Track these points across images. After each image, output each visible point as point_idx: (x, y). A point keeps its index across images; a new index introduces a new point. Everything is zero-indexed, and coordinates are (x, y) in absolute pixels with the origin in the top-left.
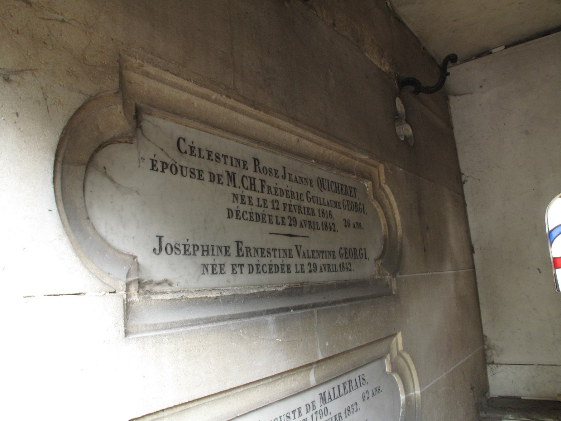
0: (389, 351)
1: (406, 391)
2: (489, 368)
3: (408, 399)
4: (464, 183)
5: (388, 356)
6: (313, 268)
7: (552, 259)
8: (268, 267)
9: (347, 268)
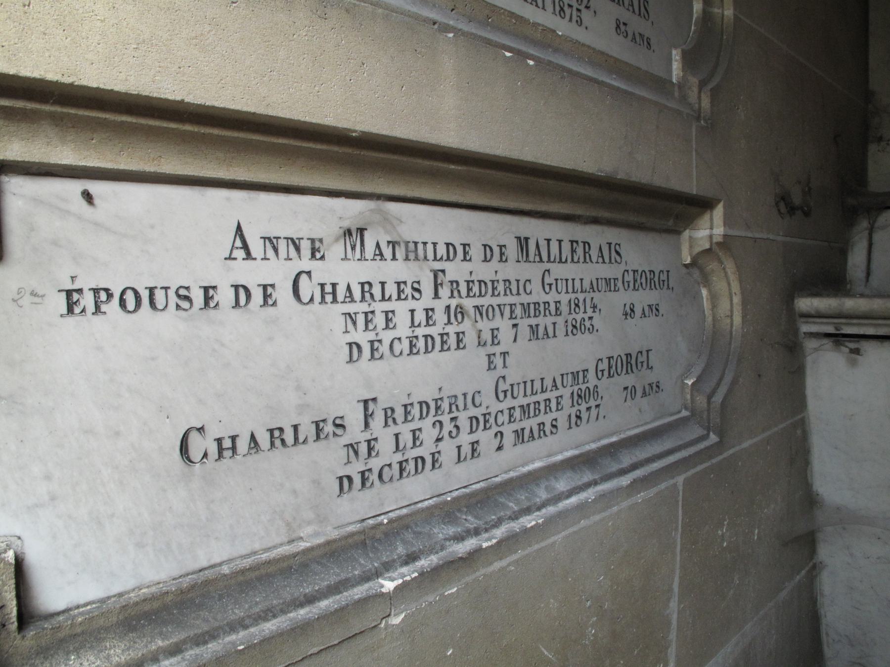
2: (873, 148)
3: (706, 16)
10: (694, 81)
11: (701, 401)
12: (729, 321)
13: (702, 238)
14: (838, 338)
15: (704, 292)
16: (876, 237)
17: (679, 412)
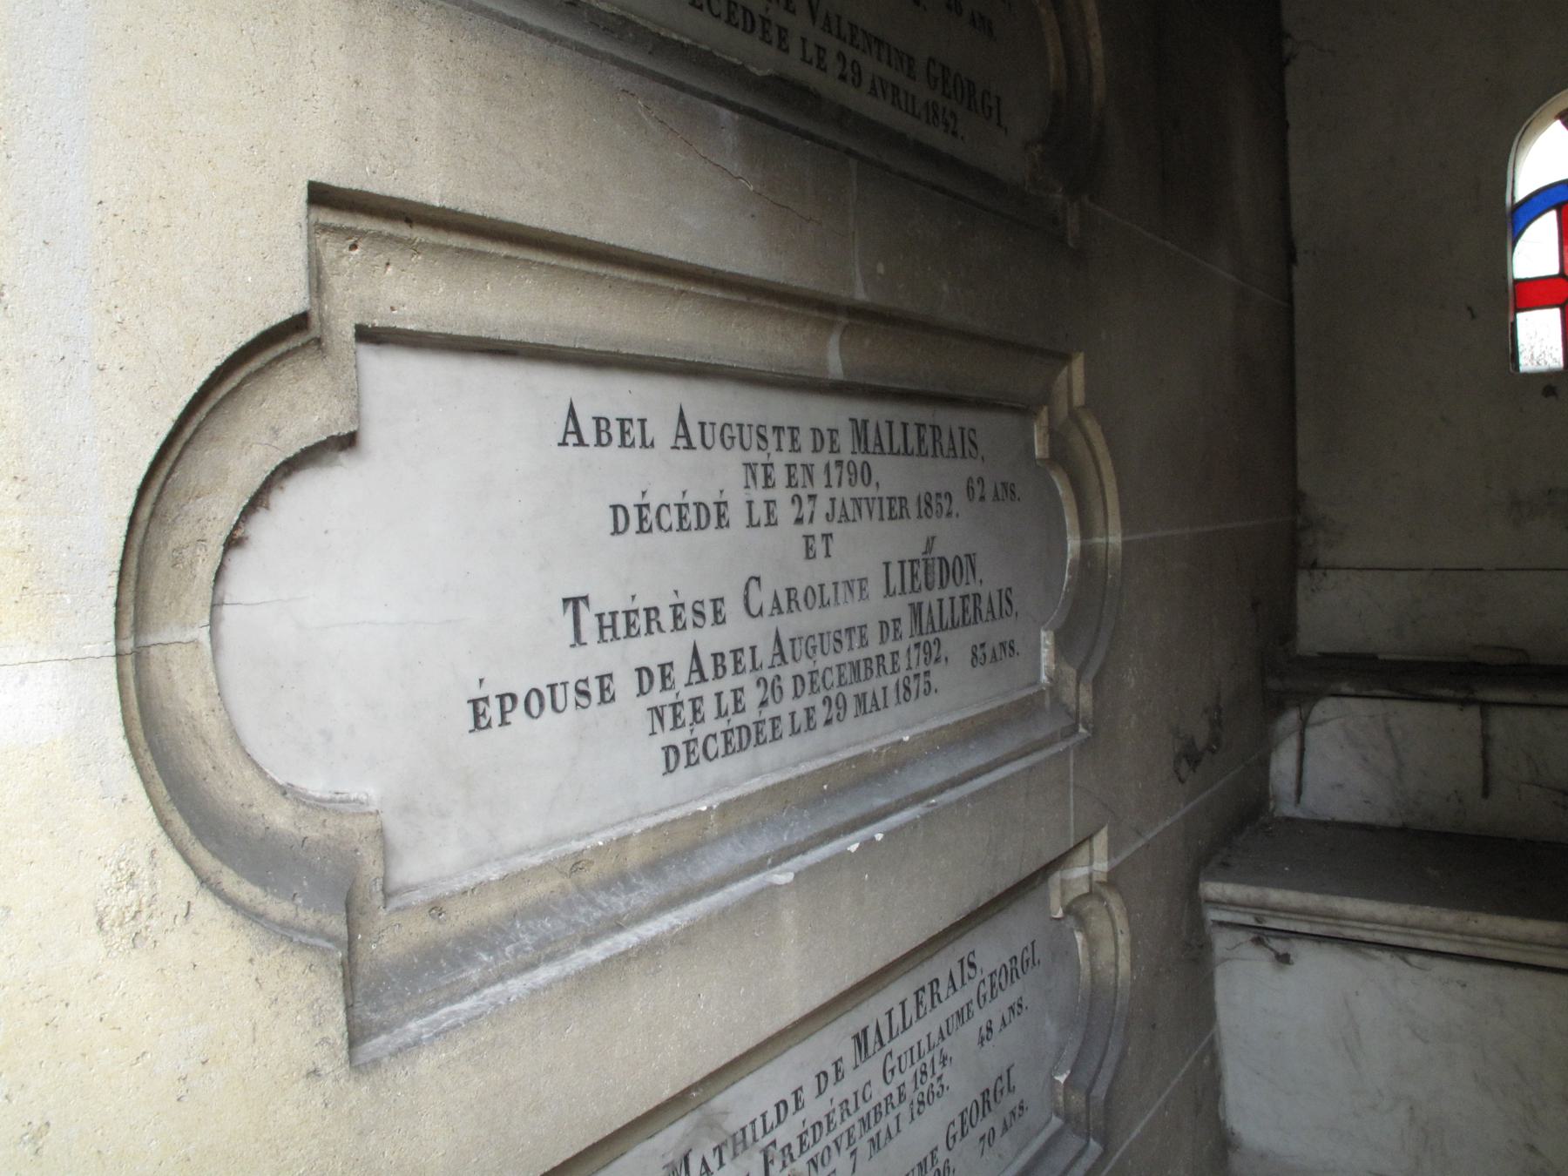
0: (1046, 398)
1: (1086, 530)
2: (1303, 579)
3: (1087, 553)
4: (1287, 62)
5: (1044, 415)
6: (851, 74)
7: (1510, 282)
8: (675, 510)
9: (947, 124)
10: (1070, 672)
11: (1077, 1100)
12: (1112, 971)
13: (1078, 879)
14: (1260, 935)
15: (1079, 937)
16: (1311, 734)
17: (1048, 1122)
